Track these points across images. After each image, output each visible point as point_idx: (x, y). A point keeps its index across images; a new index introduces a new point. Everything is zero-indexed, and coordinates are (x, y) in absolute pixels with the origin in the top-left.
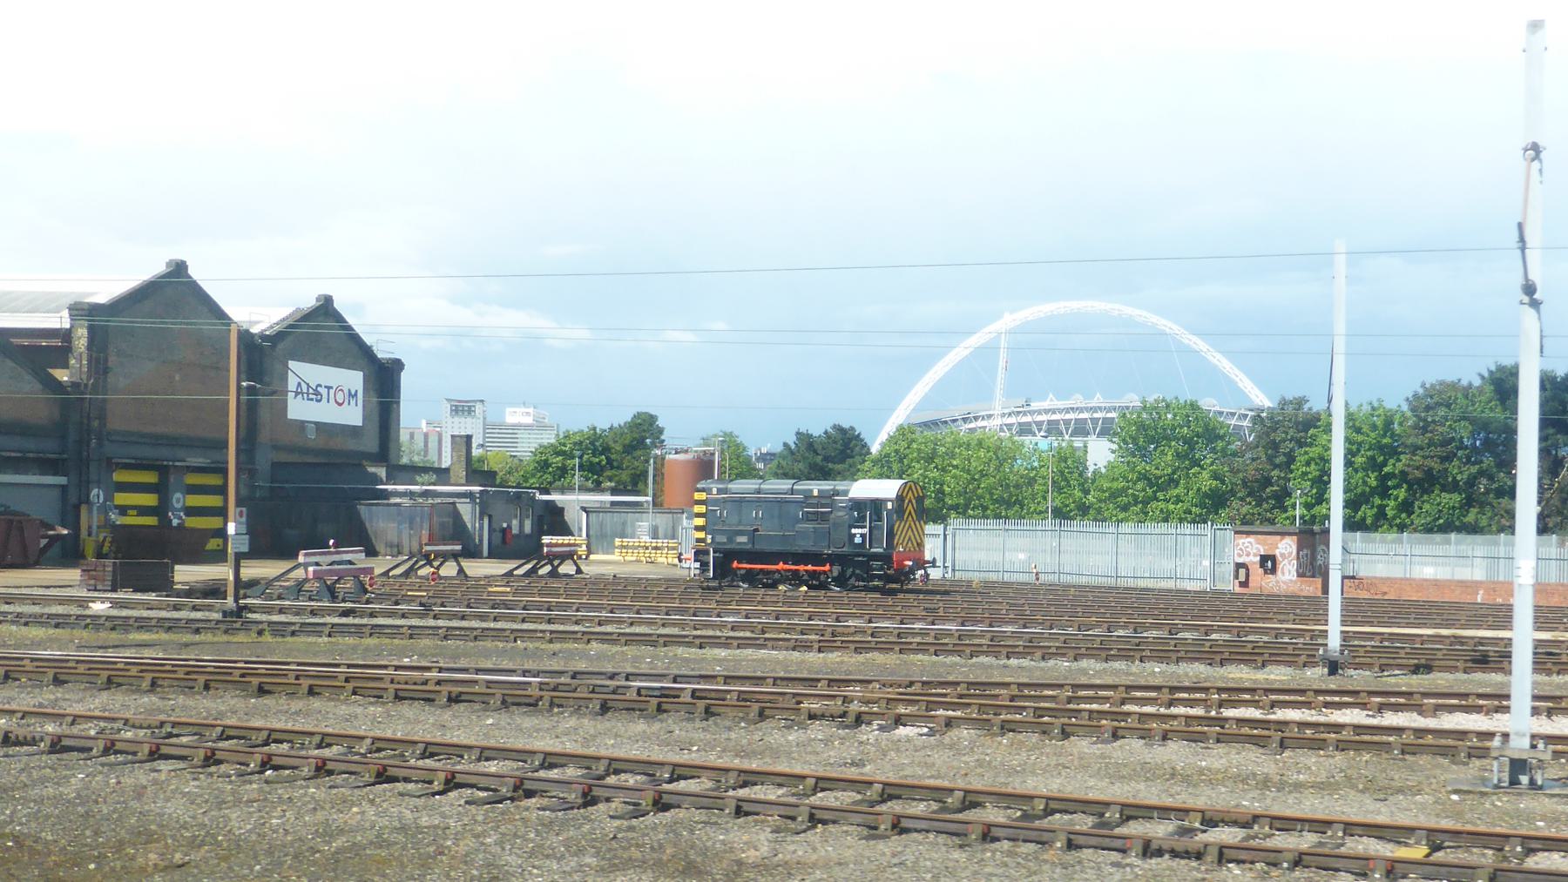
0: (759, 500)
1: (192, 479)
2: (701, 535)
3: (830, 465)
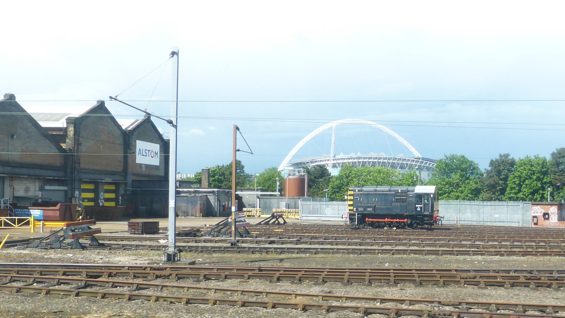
0: (376, 194)
1: (106, 187)
2: (352, 208)
3: (317, 180)
